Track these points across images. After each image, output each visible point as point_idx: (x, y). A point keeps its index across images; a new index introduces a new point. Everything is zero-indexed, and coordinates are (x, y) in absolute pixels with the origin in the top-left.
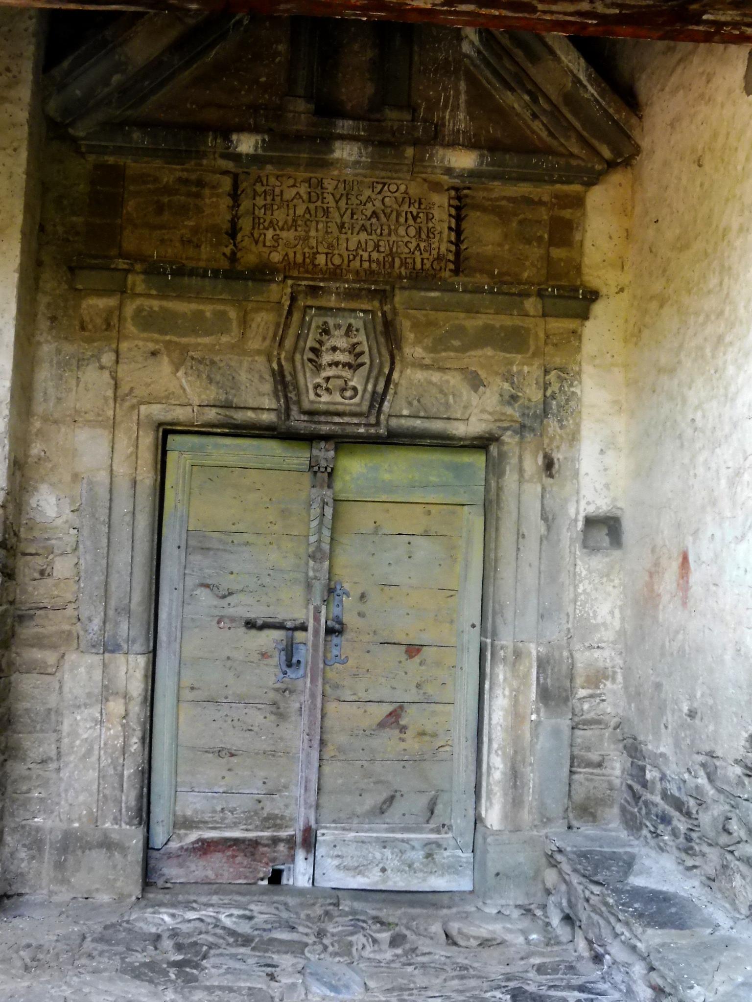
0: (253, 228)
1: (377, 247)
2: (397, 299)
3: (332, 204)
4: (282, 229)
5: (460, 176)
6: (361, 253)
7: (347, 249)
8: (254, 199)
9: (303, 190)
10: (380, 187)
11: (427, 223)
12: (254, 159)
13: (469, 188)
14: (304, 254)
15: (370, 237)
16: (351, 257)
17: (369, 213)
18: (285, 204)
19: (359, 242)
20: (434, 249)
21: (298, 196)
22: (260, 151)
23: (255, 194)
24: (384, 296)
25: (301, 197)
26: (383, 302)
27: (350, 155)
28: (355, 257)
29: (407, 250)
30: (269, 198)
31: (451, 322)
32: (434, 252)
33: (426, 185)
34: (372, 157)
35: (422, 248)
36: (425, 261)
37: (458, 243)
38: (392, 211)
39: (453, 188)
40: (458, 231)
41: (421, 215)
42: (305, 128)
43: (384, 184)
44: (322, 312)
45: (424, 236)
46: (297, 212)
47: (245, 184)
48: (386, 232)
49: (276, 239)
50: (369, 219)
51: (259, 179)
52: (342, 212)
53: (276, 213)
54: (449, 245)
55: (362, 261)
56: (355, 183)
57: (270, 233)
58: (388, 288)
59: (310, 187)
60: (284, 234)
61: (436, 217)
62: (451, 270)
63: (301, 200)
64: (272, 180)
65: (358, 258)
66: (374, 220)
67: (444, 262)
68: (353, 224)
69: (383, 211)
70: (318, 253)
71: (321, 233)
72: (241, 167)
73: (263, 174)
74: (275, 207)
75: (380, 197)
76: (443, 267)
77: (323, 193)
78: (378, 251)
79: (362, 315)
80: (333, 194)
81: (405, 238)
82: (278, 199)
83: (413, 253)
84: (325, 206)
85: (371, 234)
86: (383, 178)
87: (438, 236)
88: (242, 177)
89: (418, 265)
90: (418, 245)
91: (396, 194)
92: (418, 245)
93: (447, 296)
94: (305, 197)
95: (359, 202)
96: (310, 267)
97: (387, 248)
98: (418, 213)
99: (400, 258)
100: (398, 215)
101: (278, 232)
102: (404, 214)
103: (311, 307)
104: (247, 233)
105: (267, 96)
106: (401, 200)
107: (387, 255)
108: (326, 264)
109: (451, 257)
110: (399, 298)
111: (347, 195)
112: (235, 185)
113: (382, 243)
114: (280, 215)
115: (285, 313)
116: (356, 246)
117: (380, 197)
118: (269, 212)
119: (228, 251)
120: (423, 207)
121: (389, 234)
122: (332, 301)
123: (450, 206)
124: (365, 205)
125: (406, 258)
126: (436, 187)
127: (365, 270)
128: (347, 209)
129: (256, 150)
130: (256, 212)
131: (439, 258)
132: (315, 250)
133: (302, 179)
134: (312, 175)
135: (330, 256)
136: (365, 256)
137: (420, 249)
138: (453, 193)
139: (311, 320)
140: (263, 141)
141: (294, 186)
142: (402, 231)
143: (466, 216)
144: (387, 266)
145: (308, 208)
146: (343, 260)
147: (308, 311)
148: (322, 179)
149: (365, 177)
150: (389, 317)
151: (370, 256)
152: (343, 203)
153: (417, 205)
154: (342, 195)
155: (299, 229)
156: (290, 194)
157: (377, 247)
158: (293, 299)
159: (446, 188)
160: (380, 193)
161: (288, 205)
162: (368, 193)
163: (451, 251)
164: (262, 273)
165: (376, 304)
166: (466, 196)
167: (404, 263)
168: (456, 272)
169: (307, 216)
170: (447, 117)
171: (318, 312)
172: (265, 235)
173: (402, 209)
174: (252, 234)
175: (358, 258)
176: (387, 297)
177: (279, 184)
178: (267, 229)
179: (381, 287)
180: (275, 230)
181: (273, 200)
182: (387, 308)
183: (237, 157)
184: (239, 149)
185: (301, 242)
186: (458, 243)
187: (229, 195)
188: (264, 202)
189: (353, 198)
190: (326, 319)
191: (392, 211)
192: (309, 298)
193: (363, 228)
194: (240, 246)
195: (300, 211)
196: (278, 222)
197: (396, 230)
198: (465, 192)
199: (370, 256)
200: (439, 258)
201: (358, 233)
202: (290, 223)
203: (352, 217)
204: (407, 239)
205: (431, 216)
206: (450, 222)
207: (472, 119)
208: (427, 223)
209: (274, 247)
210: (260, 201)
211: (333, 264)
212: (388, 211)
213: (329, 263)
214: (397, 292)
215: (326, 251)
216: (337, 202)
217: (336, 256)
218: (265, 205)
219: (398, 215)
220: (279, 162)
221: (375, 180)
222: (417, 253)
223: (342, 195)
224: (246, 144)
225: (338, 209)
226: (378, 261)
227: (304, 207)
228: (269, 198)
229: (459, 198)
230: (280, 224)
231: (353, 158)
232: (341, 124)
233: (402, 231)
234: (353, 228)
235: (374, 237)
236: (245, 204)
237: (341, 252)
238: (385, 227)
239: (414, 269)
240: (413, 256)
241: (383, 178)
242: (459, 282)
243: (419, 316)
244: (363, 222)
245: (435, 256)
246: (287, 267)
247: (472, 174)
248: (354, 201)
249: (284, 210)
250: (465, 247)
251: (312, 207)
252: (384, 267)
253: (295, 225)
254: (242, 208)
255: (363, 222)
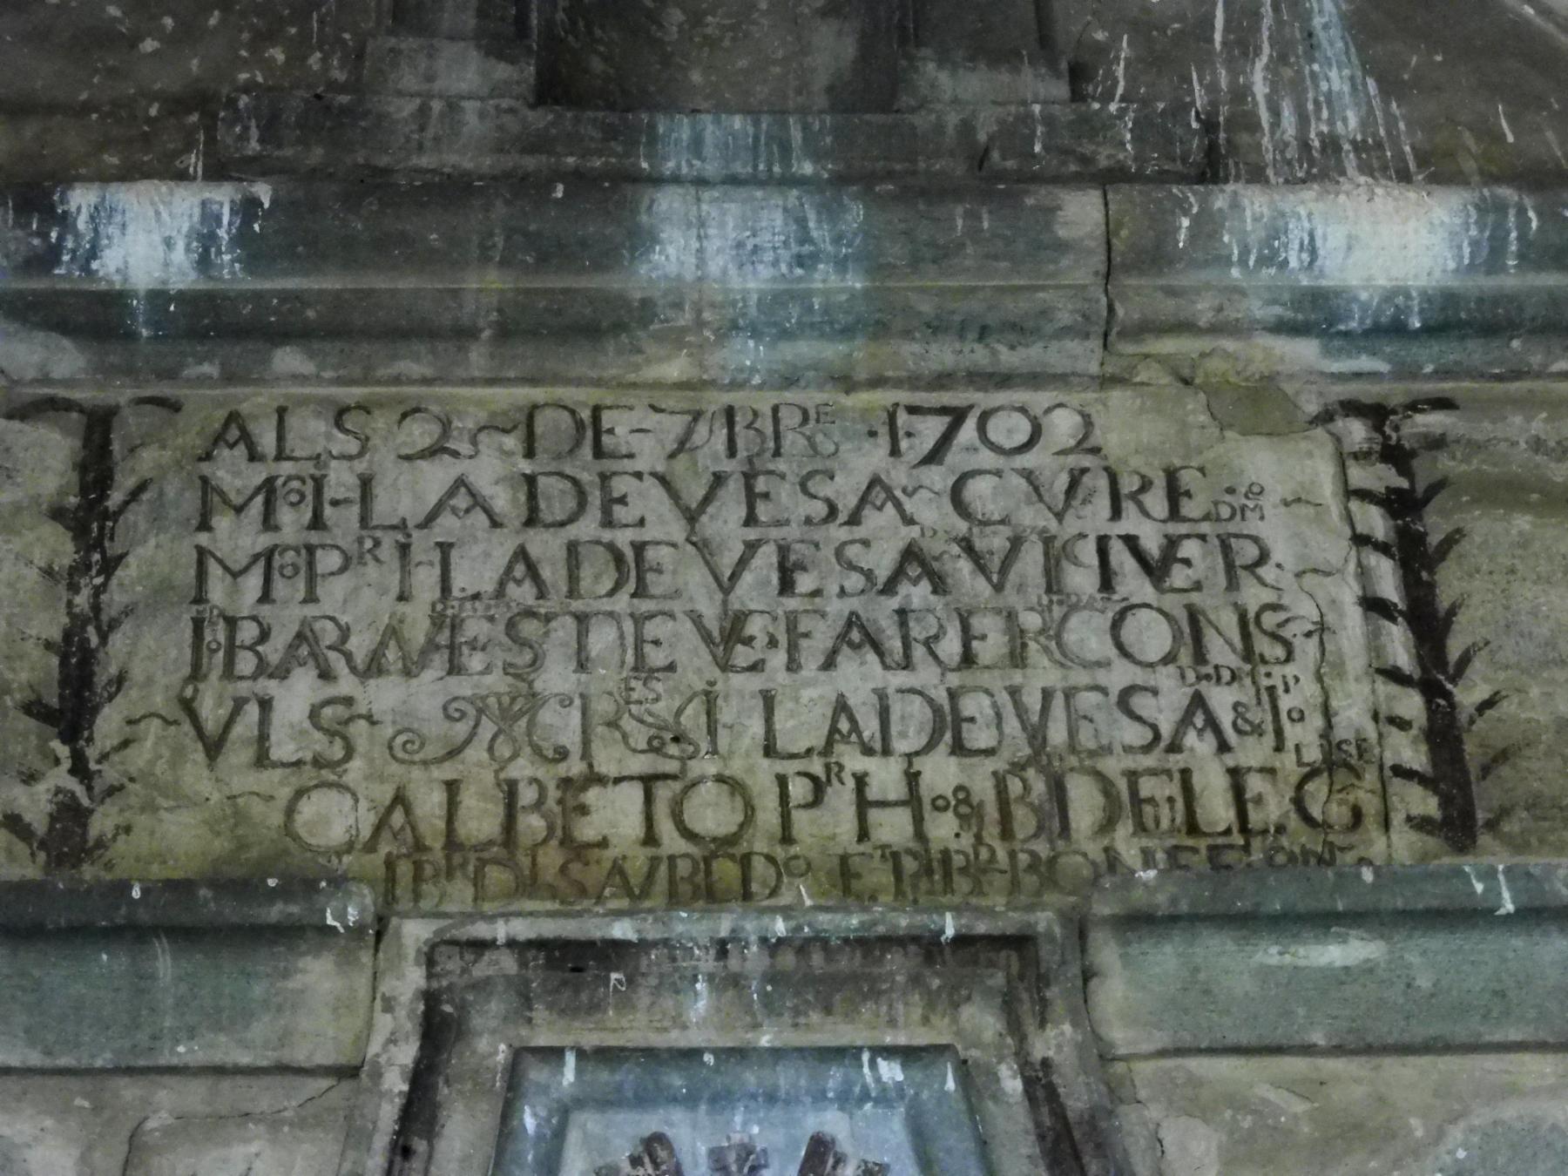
0: (197, 674)
1: (948, 728)
2: (1115, 992)
3: (664, 524)
4: (373, 668)
5: (1388, 329)
6: (854, 762)
7: (769, 750)
8: (205, 526)
9: (492, 469)
10: (931, 429)
11: (1233, 584)
12: (203, 322)
13: (1442, 403)
14: (511, 791)
15: (899, 679)
16: (799, 790)
17: (883, 561)
18: (389, 540)
19: (842, 706)
20: (1299, 717)
21: (461, 501)
22: (230, 270)
23: (210, 502)
24: (1020, 969)
25: (478, 502)
26: (1026, 1008)
27: (747, 255)
28: (819, 788)
29: (1135, 734)
30: (292, 521)
31: (1481, 1116)
32: (1305, 736)
33: (1195, 408)
34: (877, 267)
35: (1226, 719)
36: (1255, 784)
37: (1434, 675)
38: (1016, 543)
39: (1352, 408)
40: (1428, 622)
41: (1189, 549)
42: (487, 163)
43: (957, 416)
44: (627, 1077)
45: (1221, 653)
46: (461, 581)
47: (149, 459)
48: (992, 647)
49: (336, 721)
50: (889, 588)
51: (234, 430)
52: (727, 562)
53: (333, 592)
54: (1385, 688)
55: (863, 805)
56: (790, 419)
57: (296, 697)
58: (1044, 920)
59: (530, 453)
60: (384, 695)
61: (1279, 553)
62: (1421, 824)
63: (480, 519)
64: (311, 431)
65: (842, 798)
66: (917, 593)
67: (1370, 777)
68: (792, 621)
69: (968, 547)
70: (594, 779)
71: (606, 677)
72: (129, 371)
73: (256, 402)
74: (328, 561)
75: (939, 477)
76: (1371, 805)
77: (605, 478)
78: (959, 748)
79: (891, 1071)
80: (663, 480)
81: (1110, 673)
82: (342, 522)
83: (1174, 747)
84: (623, 538)
85: (907, 664)
86: (942, 380)
87: (1308, 650)
88: (131, 423)
89: (1217, 810)
90: (1198, 701)
91: (1027, 460)
92: (1198, 701)
93: (1426, 959)
94: (503, 500)
95: (820, 509)
96: (551, 858)
97: (1012, 725)
98: (1172, 543)
99: (1099, 776)
100: (1056, 558)
101: (346, 684)
102: (1088, 552)
103: (554, 1054)
104: (159, 700)
105: (278, 55)
106: (1063, 481)
107: (1018, 768)
108: (650, 839)
109: (1409, 751)
110: (1130, 991)
111: (749, 478)
112: (95, 468)
113: (972, 705)
114: (357, 601)
115: (388, 1115)
116: (815, 725)
117: (939, 477)
118: (288, 590)
119: (35, 804)
120: (1189, 508)
121: (1017, 657)
122: (699, 1016)
123: (1351, 493)
124: (854, 520)
125: (1133, 776)
126: (1258, 406)
127: (893, 857)
128: (752, 547)
129: (204, 263)
130: (217, 591)
131: (1338, 761)
132: (575, 767)
133: (483, 416)
134: (538, 394)
135: (664, 792)
136: (886, 777)
137: (1213, 724)
138: (1357, 432)
139: (557, 1138)
140: (248, 207)
141: (435, 451)
142: (1088, 634)
143: (1450, 541)
144: (1024, 821)
145: (522, 554)
146: (750, 809)
147: (536, 1074)
148: (597, 411)
149: (847, 383)
150: (1078, 1097)
151: (912, 778)
152: (726, 522)
153: (1156, 502)
154: (719, 480)
155: (476, 662)
156: (408, 491)
157: (948, 728)
158: (439, 1029)
159: (1312, 408)
160: (934, 456)
161: (404, 549)
162: (874, 458)
163: (1402, 724)
164: (245, 912)
165: (981, 1021)
166: (1437, 443)
167: (1125, 803)
168: (1457, 827)
169: (523, 594)
170: (1260, 89)
171: (604, 1076)
172: (265, 705)
173: (1071, 526)
174: (188, 707)
175: (842, 798)
176: (1043, 981)
177: (353, 446)
178: (282, 673)
179: (998, 914)
180: (326, 675)
181: (317, 523)
182: (1054, 1042)
183: (98, 317)
184: (109, 264)
185: (487, 729)
186: (1434, 675)
187: (57, 514)
188: (265, 541)
189: (786, 493)
190: (651, 1122)
191: (1016, 543)
192: (540, 1013)
193: (858, 635)
194: (110, 774)
195: (477, 570)
196: (345, 633)
197: (1054, 633)
198: (1432, 421)
199: (912, 778)
200: (1338, 761)
201: (829, 664)
202: (418, 629)
203: (787, 586)
204: (1120, 675)
205: (1250, 552)
206: (1363, 573)
207: (1391, 87)
208: (1233, 584)
209: (318, 762)
210: (236, 537)
211: (689, 835)
212: (994, 542)
213: (666, 828)
214: (1106, 952)
215: (641, 764)
216: (692, 517)
217: (708, 790)
218: (268, 555)
219: (1056, 558)
220: (332, 329)
221: (904, 397)
222: (1199, 745)
223: (719, 480)
224: (148, 237)
225: (704, 548)
226: (963, 804)
227: (502, 548)
228: (292, 521)
229: (1395, 455)
230: (360, 645)
231: (757, 281)
232: (685, 134)
233: (1088, 634)
234: (795, 637)
235: (925, 675)
236: (150, 554)
237: (736, 768)
238: (988, 624)
239: (1193, 828)
240: (1176, 761)
241: (942, 380)
242: (1489, 873)
243: (1265, 1091)
244: (854, 604)
245: (1313, 754)
246: (404, 869)
247: (1450, 317)
248: (788, 502)
249: (383, 573)
250: (1481, 693)
251: (547, 546)
252: (1007, 833)
253: (448, 644)
254: (128, 572)
255: (854, 604)
